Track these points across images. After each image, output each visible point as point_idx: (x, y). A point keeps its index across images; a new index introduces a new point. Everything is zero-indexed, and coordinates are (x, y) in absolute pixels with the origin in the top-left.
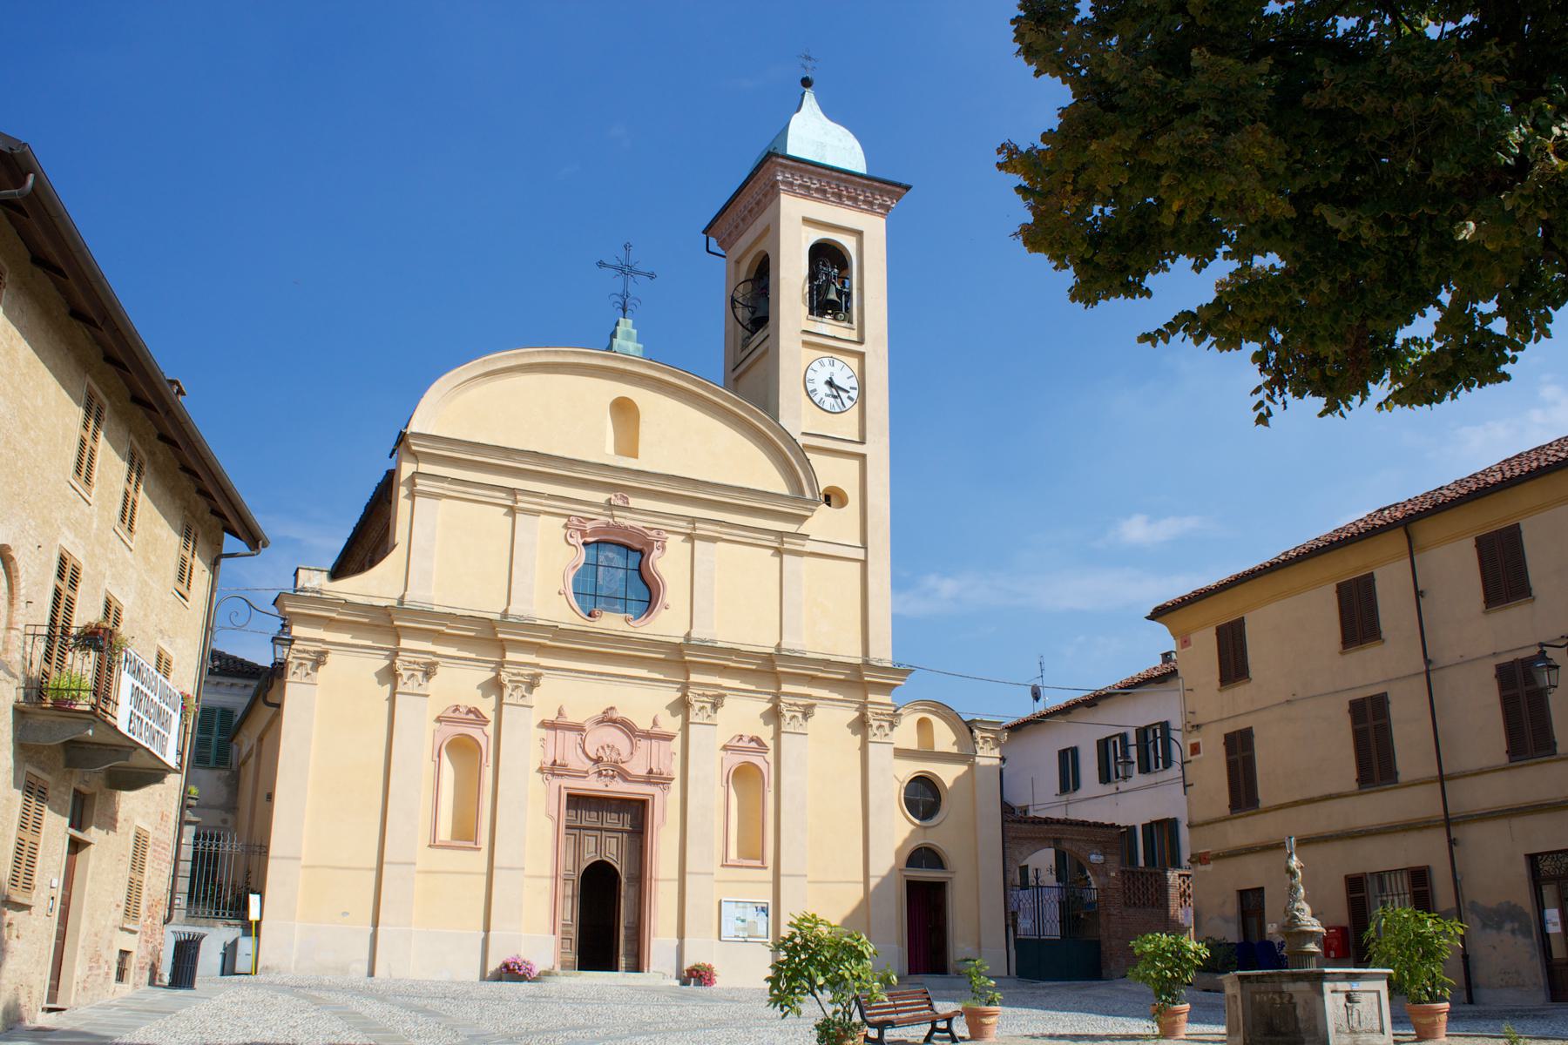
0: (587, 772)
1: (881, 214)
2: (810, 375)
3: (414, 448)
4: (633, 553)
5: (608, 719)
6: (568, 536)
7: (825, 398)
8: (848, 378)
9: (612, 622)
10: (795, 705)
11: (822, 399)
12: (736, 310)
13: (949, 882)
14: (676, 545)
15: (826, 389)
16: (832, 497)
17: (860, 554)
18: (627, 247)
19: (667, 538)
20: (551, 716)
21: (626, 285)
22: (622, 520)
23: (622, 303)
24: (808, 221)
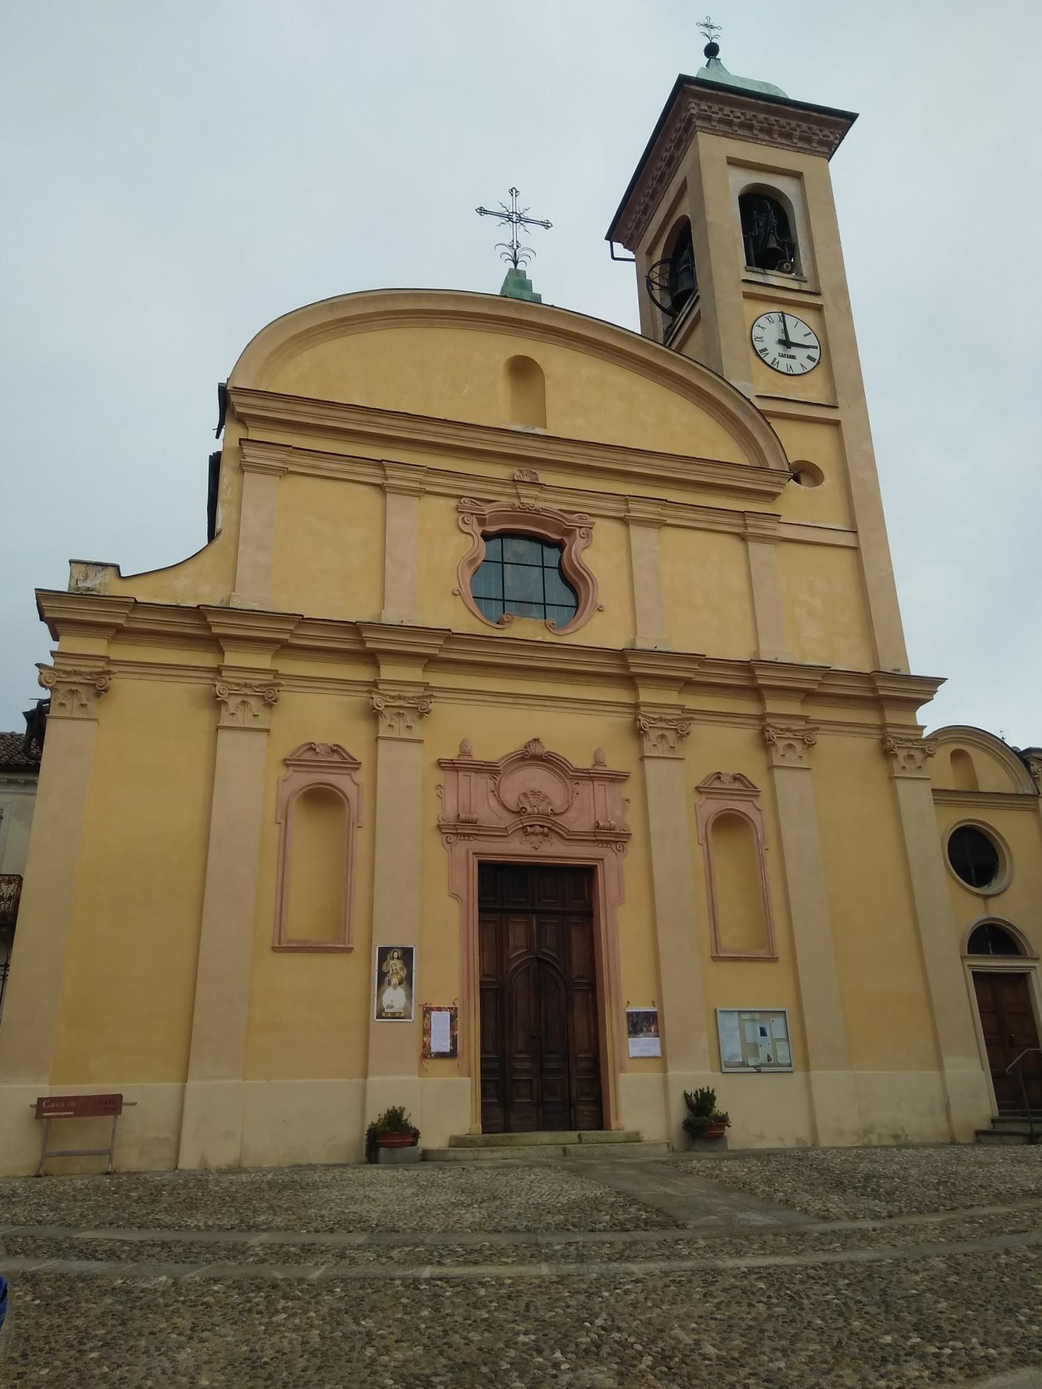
0: (506, 829)
1: (823, 152)
2: (757, 332)
3: (239, 409)
4: (656, 1055)
5: (532, 756)
6: (461, 525)
7: (779, 359)
8: (805, 335)
9: (527, 628)
10: (789, 730)
11: (775, 359)
12: (653, 292)
13: (1032, 973)
14: (606, 532)
15: (781, 349)
16: (804, 472)
17: (847, 540)
18: (513, 192)
19: (594, 523)
20: (452, 754)
21: (514, 233)
22: (531, 501)
23: (512, 255)
24: (733, 162)
